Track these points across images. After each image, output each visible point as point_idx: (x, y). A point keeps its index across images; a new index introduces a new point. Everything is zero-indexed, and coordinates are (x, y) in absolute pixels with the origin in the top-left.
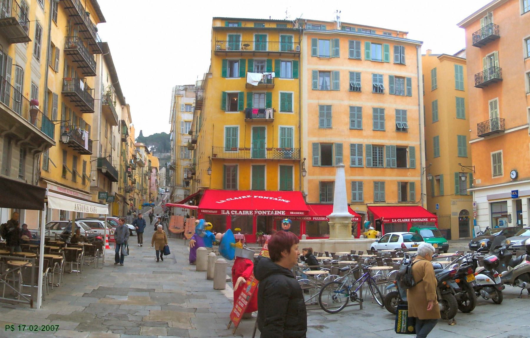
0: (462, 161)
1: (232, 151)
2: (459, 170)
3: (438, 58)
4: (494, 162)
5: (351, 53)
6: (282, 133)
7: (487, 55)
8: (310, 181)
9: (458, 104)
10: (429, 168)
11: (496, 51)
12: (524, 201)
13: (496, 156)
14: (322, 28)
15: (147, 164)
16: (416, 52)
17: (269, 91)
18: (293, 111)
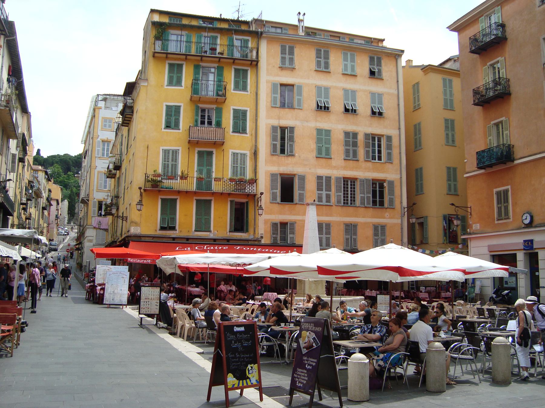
0: (452, 199)
1: (170, 181)
2: (451, 211)
3: (422, 69)
4: (499, 202)
5: (318, 64)
6: (234, 160)
7: (488, 64)
8: (266, 221)
9: (447, 127)
10: (412, 207)
11: (502, 57)
13: (501, 194)
14: (284, 32)
15: (45, 195)
16: (395, 62)
17: (220, 106)
18: (247, 132)
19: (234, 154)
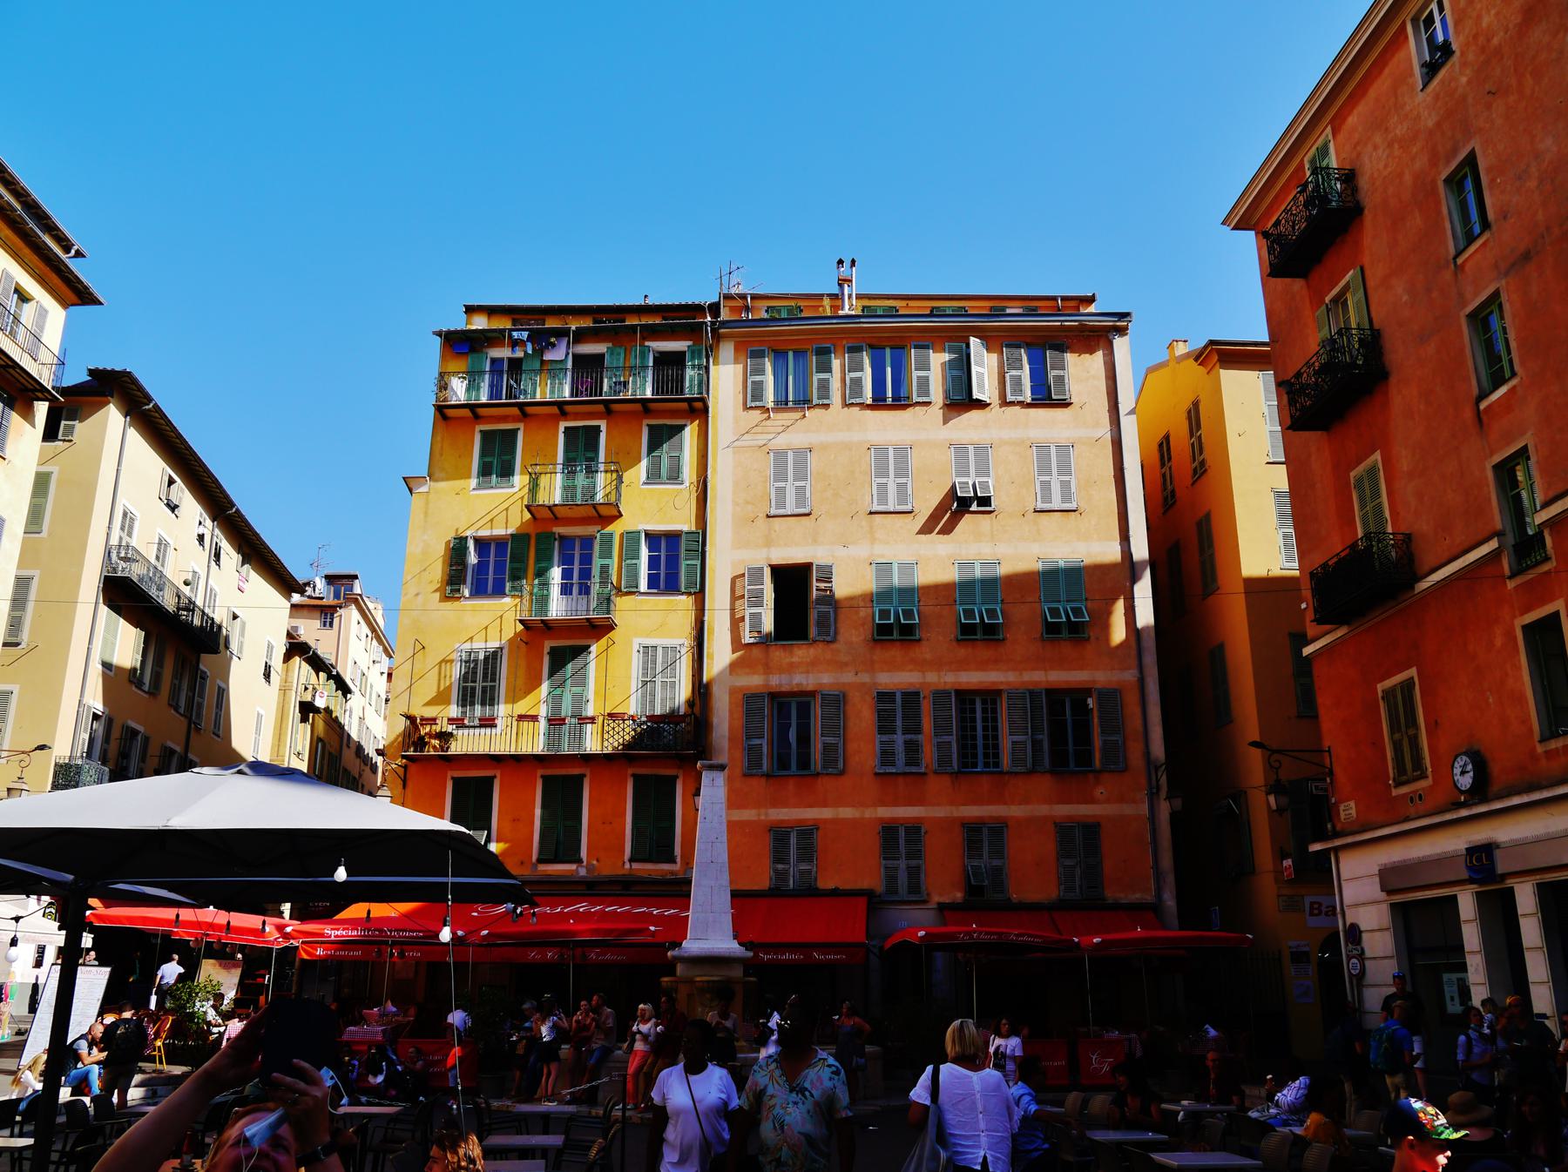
1: (483, 730)
6: (645, 663)
12: (1526, 898)
19: (648, 651)
